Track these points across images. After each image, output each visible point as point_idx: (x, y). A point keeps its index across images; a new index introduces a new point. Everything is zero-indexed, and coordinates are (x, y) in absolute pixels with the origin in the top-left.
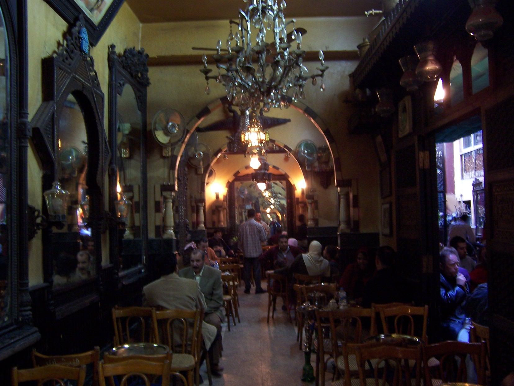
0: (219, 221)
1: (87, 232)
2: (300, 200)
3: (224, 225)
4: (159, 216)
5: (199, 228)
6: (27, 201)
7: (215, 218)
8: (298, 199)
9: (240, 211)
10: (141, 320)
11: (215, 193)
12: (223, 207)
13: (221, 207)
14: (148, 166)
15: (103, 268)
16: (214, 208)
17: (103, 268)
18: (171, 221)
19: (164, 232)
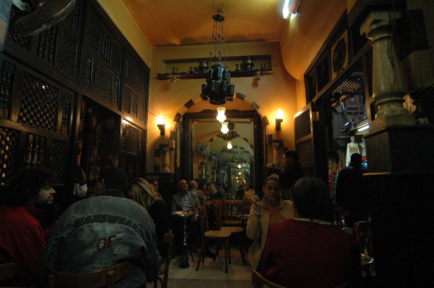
0: (164, 166)
1: (28, 149)
2: (274, 138)
3: (170, 170)
4: (222, 180)
5: (203, 178)
6: (177, 165)
7: (158, 161)
8: (270, 136)
9: (212, 171)
10: (255, 177)
11: (164, 124)
12: (170, 147)
13: (167, 146)
14: (174, 129)
15: (75, 184)
16: (157, 148)
17: (75, 184)
18: (215, 178)
19: (214, 180)
